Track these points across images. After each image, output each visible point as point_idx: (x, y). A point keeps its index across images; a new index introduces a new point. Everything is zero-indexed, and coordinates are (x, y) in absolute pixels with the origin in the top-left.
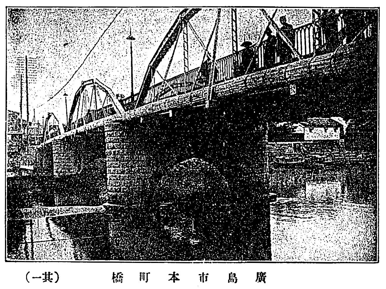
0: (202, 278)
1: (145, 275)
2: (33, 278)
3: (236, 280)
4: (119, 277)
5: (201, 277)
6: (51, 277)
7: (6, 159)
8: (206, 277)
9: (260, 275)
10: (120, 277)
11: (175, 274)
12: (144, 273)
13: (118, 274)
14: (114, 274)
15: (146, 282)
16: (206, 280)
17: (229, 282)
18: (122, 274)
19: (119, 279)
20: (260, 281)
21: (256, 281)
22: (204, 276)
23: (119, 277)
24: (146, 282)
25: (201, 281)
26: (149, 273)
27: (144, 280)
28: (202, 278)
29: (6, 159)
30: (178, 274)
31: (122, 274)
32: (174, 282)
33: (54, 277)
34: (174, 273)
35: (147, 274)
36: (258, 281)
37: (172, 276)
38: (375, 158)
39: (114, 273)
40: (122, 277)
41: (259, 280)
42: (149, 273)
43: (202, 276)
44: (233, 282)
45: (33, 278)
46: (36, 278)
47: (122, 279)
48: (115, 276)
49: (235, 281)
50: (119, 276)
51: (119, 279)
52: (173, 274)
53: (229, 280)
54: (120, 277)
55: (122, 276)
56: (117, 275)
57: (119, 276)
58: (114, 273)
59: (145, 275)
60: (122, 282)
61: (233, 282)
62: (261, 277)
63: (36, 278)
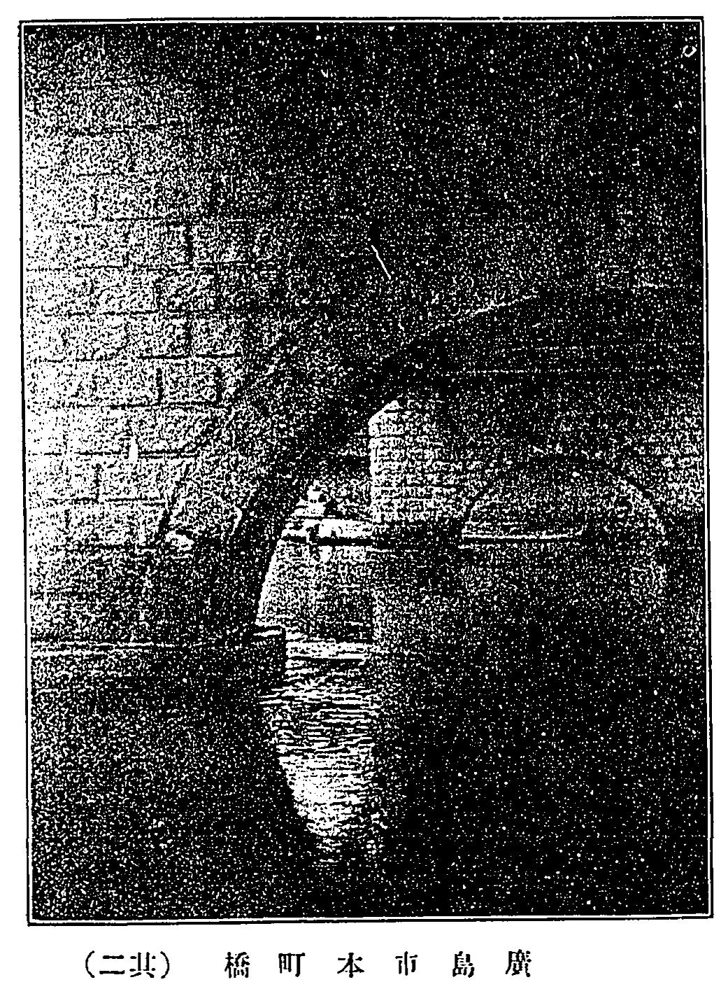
0: (403, 965)
1: (294, 959)
2: (106, 957)
3: (473, 969)
4: (240, 964)
5: (400, 962)
6: (152, 963)
7: (26, 657)
8: (414, 962)
9: (517, 957)
10: (244, 963)
11: (354, 957)
12: (290, 955)
13: (240, 955)
14: (229, 958)
15: (298, 975)
16: (413, 970)
17: (454, 974)
18: (247, 957)
19: (240, 968)
20: (516, 972)
21: (507, 973)
22: (409, 961)
23: (240, 964)
24: (298, 975)
25: (400, 972)
26: (303, 954)
27: (290, 970)
28: (403, 965)
29: (26, 657)
30: (360, 959)
31: (247, 957)
32: (351, 976)
33: (159, 965)
34: (351, 955)
35: (299, 956)
36: (511, 971)
37: (346, 961)
38: (37, 905)
39: (229, 954)
40: (248, 964)
41: (514, 969)
42: (303, 954)
43: (403, 960)
44: (465, 974)
45: (106, 957)
46: (114, 957)
47: (247, 969)
48: (233, 961)
49: (469, 971)
50: (240, 961)
51: (240, 968)
52: (347, 957)
53: (454, 970)
54: (244, 963)
55: (246, 960)
56: (237, 959)
57: (240, 961)
58: (229, 954)
59: (294, 959)
60: (247, 976)
61: (465, 974)
62: (518, 962)
63: (114, 957)
